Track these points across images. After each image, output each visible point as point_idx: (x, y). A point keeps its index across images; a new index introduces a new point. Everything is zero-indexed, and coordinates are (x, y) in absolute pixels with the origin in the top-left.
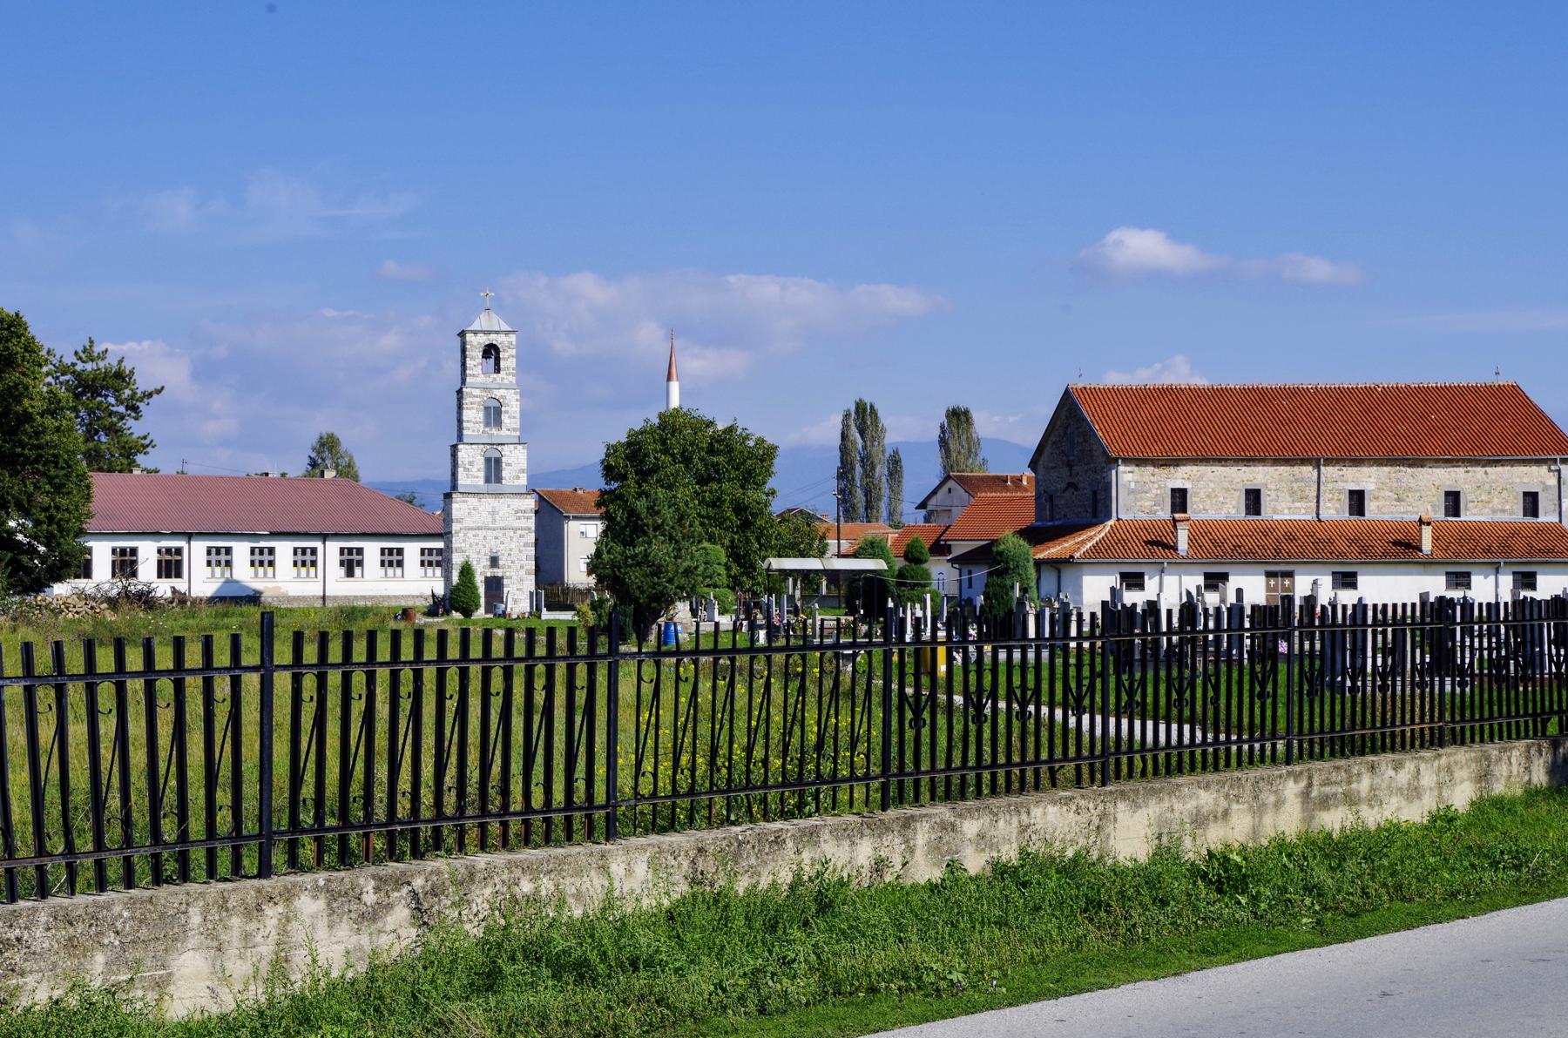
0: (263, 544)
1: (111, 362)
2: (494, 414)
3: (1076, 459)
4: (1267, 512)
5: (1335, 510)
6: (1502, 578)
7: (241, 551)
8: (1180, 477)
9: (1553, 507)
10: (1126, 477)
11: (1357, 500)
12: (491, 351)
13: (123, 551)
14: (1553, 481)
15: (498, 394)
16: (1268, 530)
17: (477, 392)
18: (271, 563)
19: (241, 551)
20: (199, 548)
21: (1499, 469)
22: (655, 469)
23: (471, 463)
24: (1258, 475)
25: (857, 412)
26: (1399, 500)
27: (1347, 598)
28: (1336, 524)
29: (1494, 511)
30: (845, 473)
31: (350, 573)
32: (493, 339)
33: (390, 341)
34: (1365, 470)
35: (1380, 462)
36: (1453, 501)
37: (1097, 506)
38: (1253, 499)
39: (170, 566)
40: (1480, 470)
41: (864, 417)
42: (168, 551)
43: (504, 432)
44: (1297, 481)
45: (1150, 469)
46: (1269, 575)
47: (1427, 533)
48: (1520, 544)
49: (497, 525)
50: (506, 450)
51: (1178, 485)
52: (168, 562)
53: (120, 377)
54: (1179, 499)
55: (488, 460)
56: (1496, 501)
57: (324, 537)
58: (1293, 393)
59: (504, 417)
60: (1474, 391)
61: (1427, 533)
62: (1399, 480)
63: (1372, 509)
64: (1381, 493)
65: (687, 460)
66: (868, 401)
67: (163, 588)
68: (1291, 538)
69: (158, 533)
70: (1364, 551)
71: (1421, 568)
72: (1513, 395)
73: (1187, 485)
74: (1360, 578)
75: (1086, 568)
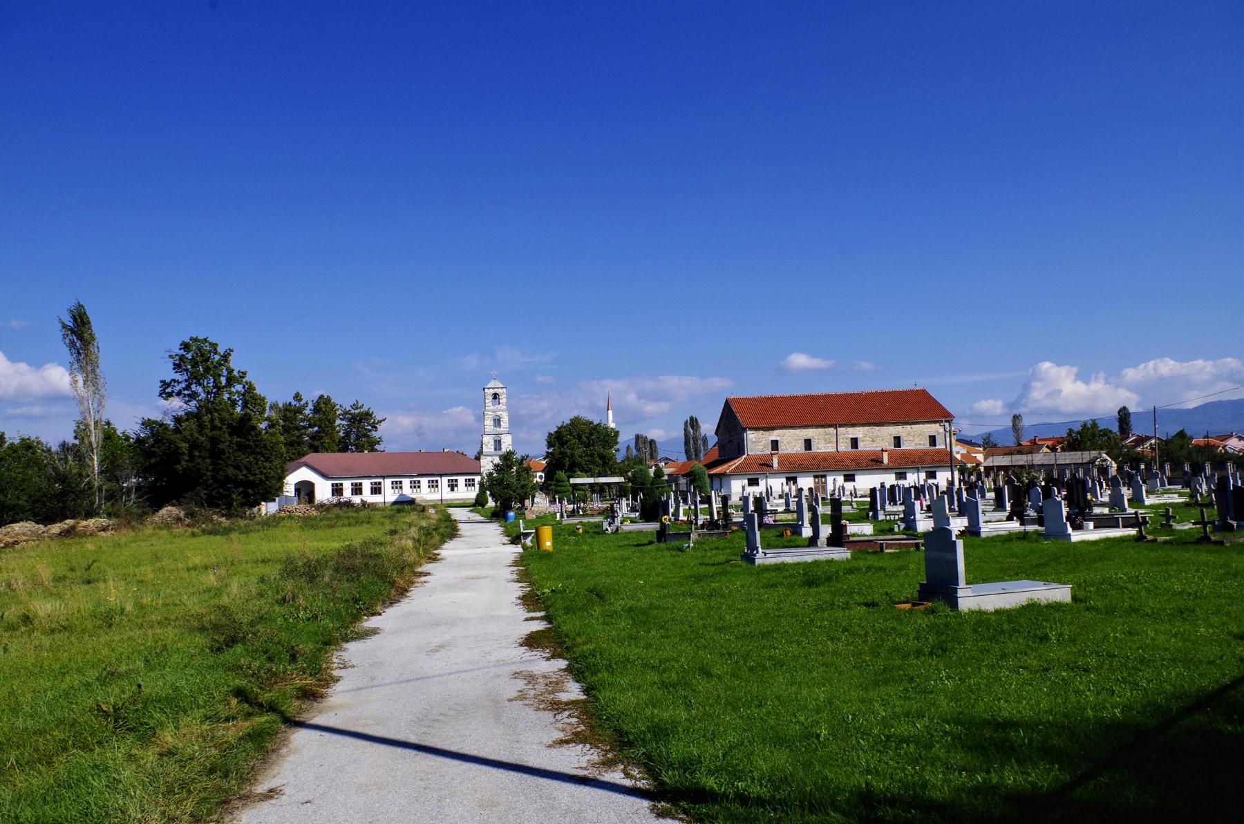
1: (365, 409)
2: (497, 422)
3: (732, 426)
4: (815, 449)
5: (845, 447)
7: (406, 482)
8: (775, 435)
10: (751, 436)
11: (854, 442)
12: (495, 396)
14: (942, 430)
16: (815, 457)
19: (406, 482)
20: (388, 482)
22: (566, 443)
24: (810, 433)
27: (849, 486)
30: (687, 443)
31: (452, 490)
33: (544, 404)
35: (864, 425)
36: (897, 441)
37: (739, 450)
38: (808, 444)
39: (376, 490)
40: (909, 427)
41: (693, 423)
46: (815, 477)
47: (885, 455)
48: (929, 459)
53: (368, 415)
54: (775, 445)
57: (441, 476)
58: (826, 397)
60: (905, 392)
61: (885, 455)
65: (580, 438)
67: (357, 500)
68: (825, 460)
70: (858, 464)
72: (923, 393)
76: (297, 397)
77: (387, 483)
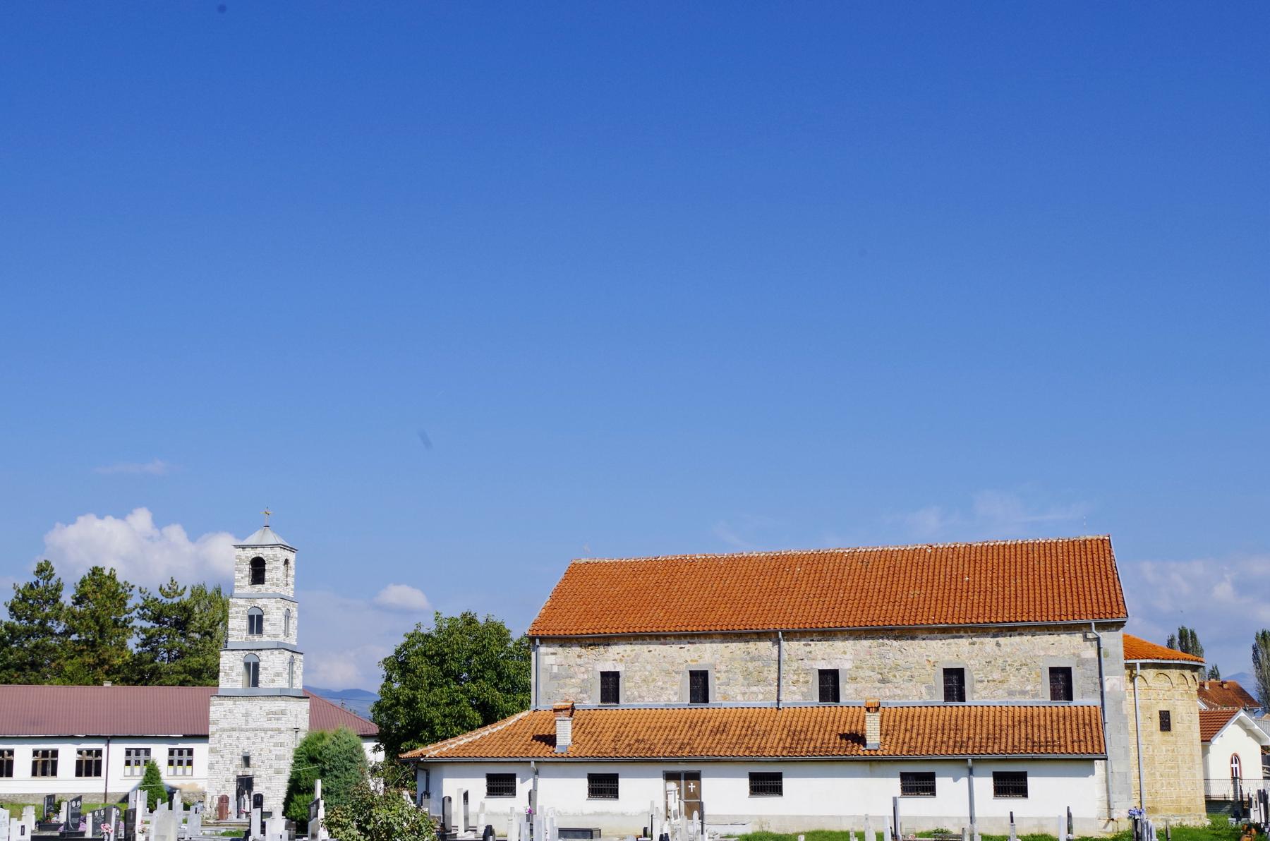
0: (181, 746)
6: (977, 781)
8: (611, 658)
9: (1092, 686)
13: (45, 753)
14: (1090, 653)
15: (260, 603)
17: (241, 602)
18: (190, 763)
19: (160, 753)
21: (1016, 639)
23: (231, 668)
24: (705, 655)
25: (1181, 637)
26: (883, 681)
28: (797, 710)
29: (1011, 693)
32: (260, 553)
34: (839, 644)
38: (700, 684)
40: (989, 643)
42: (89, 752)
43: (265, 638)
44: (753, 659)
45: (576, 650)
49: (252, 725)
50: (263, 655)
51: (609, 667)
52: (89, 763)
55: (247, 665)
56: (1013, 680)
59: (266, 625)
62: (882, 656)
63: (848, 692)
64: (861, 673)
66: (1188, 628)
69: (72, 737)
71: (866, 768)
73: (619, 668)
74: (1030, 780)
75: (446, 769)
76: (44, 570)
77: (115, 754)
